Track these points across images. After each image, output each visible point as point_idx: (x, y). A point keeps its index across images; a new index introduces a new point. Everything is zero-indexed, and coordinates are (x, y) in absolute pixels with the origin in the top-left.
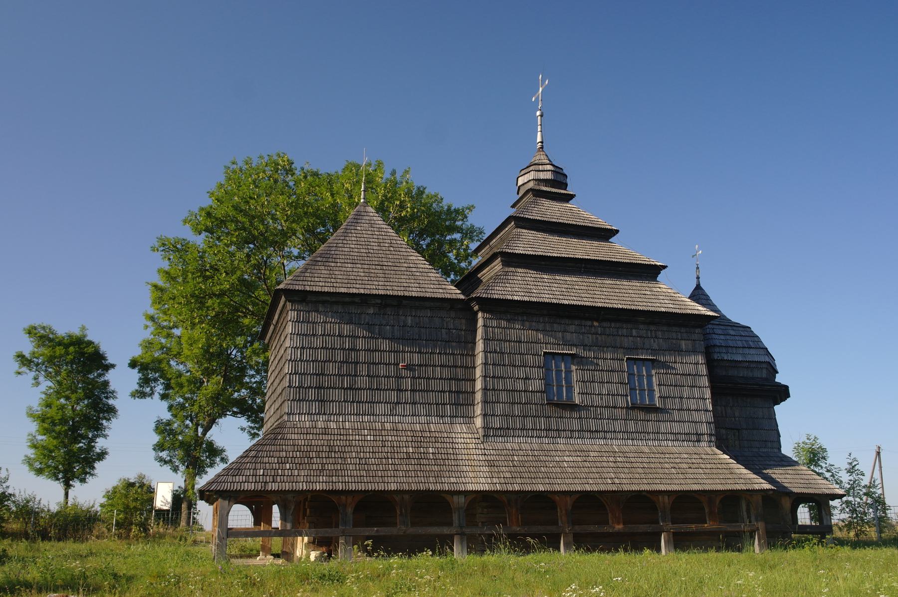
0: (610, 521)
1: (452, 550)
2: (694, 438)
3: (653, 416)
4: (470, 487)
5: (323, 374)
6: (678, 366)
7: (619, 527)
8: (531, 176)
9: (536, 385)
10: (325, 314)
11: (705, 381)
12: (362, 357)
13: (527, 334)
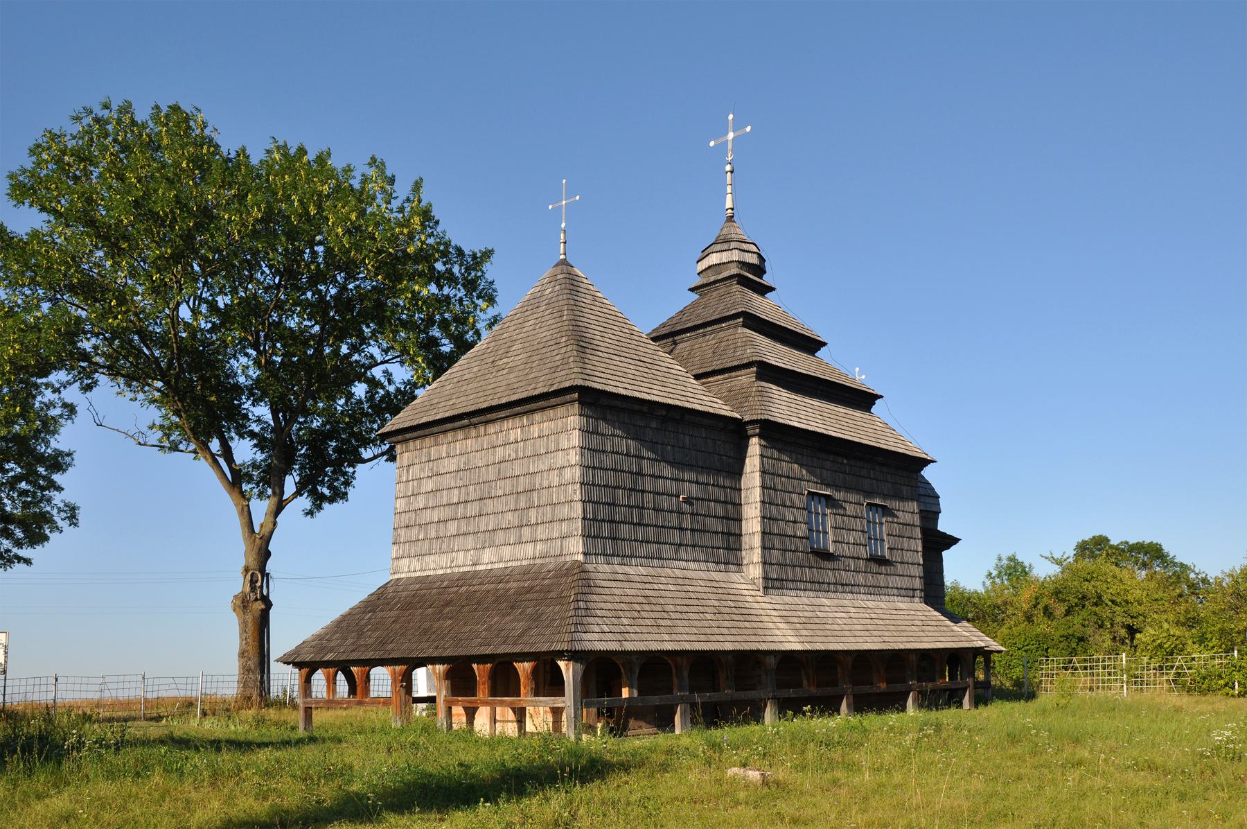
0: (805, 682)
2: (911, 593)
3: (883, 569)
4: (588, 646)
5: (614, 504)
6: (900, 514)
8: (735, 256)
9: (801, 530)
11: (918, 533)
12: (648, 483)
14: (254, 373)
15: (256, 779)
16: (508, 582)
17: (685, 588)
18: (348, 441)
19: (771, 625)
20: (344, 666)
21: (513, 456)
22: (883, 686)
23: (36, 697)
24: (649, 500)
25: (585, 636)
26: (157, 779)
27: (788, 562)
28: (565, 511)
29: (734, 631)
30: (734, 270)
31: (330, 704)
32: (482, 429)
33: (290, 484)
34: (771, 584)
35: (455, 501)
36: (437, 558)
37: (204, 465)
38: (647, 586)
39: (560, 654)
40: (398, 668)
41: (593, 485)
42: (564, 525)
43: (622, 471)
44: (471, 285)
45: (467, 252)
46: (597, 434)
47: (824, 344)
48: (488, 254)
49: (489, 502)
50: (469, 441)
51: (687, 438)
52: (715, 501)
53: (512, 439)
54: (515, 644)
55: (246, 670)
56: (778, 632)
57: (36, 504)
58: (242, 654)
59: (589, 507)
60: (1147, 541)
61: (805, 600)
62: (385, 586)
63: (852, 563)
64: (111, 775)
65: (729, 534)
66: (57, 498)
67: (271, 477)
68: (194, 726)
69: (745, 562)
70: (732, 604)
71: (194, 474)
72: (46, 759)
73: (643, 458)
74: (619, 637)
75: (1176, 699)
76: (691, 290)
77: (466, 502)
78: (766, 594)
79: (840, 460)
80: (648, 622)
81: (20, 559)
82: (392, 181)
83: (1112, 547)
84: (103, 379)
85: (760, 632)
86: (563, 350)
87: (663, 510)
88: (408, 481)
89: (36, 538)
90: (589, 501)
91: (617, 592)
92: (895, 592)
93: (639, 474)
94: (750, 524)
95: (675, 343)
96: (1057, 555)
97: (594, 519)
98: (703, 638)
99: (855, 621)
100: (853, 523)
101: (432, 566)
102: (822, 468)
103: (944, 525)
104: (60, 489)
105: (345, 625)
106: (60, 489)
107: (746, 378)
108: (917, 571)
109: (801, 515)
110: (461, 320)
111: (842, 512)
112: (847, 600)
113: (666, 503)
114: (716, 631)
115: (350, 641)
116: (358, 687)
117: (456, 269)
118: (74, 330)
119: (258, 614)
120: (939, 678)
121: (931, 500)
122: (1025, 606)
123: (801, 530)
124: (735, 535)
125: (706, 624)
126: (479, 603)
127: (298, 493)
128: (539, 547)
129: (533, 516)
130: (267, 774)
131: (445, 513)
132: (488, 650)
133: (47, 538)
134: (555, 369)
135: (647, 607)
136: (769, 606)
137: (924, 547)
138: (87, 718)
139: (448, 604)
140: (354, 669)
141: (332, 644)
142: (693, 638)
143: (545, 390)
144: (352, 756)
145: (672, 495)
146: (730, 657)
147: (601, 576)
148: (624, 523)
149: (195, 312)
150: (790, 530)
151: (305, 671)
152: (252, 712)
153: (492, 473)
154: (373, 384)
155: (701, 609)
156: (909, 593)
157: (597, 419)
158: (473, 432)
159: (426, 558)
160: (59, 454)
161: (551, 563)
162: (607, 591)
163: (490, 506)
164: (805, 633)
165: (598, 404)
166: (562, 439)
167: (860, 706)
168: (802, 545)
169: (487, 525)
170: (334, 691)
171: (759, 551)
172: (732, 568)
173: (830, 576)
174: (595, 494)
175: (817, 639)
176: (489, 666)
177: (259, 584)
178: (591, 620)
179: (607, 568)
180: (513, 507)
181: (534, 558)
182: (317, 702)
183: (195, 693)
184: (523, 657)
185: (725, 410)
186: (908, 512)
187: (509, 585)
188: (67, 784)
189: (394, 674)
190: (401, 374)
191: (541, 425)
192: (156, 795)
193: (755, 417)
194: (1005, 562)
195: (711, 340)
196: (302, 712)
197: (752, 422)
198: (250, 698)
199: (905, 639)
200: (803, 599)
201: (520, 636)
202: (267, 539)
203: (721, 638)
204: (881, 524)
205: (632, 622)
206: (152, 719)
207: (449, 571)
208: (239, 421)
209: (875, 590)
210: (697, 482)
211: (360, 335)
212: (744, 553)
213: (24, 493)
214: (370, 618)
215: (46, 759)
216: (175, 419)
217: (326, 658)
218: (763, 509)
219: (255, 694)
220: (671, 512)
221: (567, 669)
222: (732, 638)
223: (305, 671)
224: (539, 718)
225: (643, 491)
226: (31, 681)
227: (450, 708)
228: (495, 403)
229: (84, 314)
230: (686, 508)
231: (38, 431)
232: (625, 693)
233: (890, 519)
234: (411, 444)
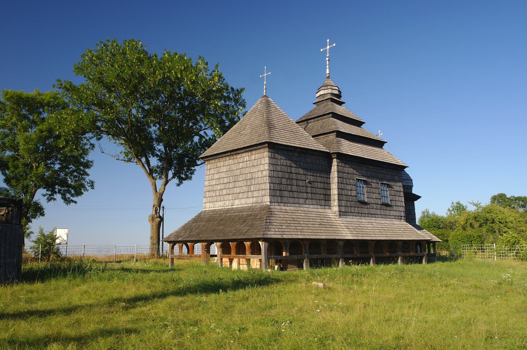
0: (355, 252)
1: (338, 265)
2: (400, 218)
3: (388, 208)
4: (269, 236)
6: (394, 187)
7: (388, 254)
8: (330, 91)
10: (280, 154)
11: (402, 194)
12: (294, 176)
13: (351, 170)
14: (158, 132)
15: (148, 282)
17: (308, 215)
18: (192, 158)
19: (341, 229)
20: (185, 243)
22: (388, 254)
23: (77, 253)
24: (294, 182)
25: (269, 233)
26: (115, 281)
28: (263, 186)
29: (326, 231)
30: (329, 96)
31: (180, 257)
32: (235, 156)
33: (170, 174)
34: (341, 214)
36: (219, 203)
37: (139, 166)
39: (259, 239)
40: (204, 244)
44: (236, 101)
45: (235, 89)
47: (364, 123)
48: (242, 90)
51: (309, 160)
52: (320, 182)
53: (245, 160)
54: (244, 235)
55: (153, 244)
56: (344, 232)
57: (80, 181)
58: (151, 238)
59: (272, 185)
60: (523, 196)
61: (356, 220)
62: (201, 213)
63: (375, 206)
64: (100, 280)
65: (326, 195)
66: (87, 178)
67: (163, 171)
68: (132, 265)
70: (326, 221)
71: (136, 171)
72: (80, 273)
75: (517, 263)
76: (314, 104)
78: (340, 218)
79: (369, 167)
80: (293, 228)
81: (73, 201)
82: (207, 64)
83: (507, 198)
84: (104, 136)
85: (337, 232)
89: (79, 193)
91: (282, 216)
92: (393, 217)
93: (291, 173)
95: (308, 123)
96: (475, 202)
97: (274, 189)
98: (314, 234)
99: (376, 228)
101: (217, 206)
102: (362, 170)
103: (415, 191)
104: (88, 175)
105: (186, 227)
106: (88, 175)
107: (332, 137)
108: (403, 209)
109: (354, 188)
110: (234, 112)
111: (370, 186)
112: (373, 220)
114: (319, 231)
115: (187, 234)
116: (190, 250)
117: (231, 95)
118: (95, 120)
119: (158, 222)
120: (413, 252)
121: (409, 181)
122: (462, 223)
123: (354, 193)
124: (328, 195)
125: (315, 228)
126: (233, 220)
127: (173, 177)
128: (255, 199)
129: (252, 188)
130: (152, 280)
131: (222, 186)
132: (235, 237)
133: (82, 193)
134: (260, 136)
135: (293, 222)
136: (341, 222)
137: (405, 200)
138: (94, 261)
139: (222, 220)
140: (189, 244)
141: (181, 234)
142: (310, 234)
143: (256, 143)
144: (183, 275)
146: (325, 241)
147: (276, 210)
149: (138, 112)
150: (349, 193)
151: (172, 244)
152: (155, 260)
153: (238, 172)
154: (201, 137)
155: (314, 223)
156: (399, 218)
158: (232, 157)
160: (88, 161)
161: (258, 205)
162: (278, 216)
163: (238, 184)
164: (355, 232)
165: (274, 148)
166: (262, 160)
167: (378, 262)
168: (354, 199)
170: (182, 252)
171: (337, 201)
172: (327, 207)
173: (366, 211)
174: (274, 180)
176: (235, 243)
178: (271, 227)
179: (278, 207)
182: (176, 256)
183: (135, 254)
184: (247, 240)
185: (323, 149)
186: (398, 187)
188: (86, 282)
189: (202, 245)
190: (210, 133)
191: (255, 155)
192: (115, 286)
193: (334, 152)
194: (455, 204)
195: (320, 122)
196: (170, 260)
198: (154, 255)
200: (355, 219)
201: (246, 232)
202: (162, 195)
203: (321, 234)
204: (387, 191)
205: (287, 227)
206: (118, 262)
208: (152, 150)
209: (384, 216)
210: (313, 176)
211: (196, 119)
213: (75, 176)
215: (80, 273)
216: (130, 150)
218: (338, 185)
219: (156, 254)
222: (325, 234)
223: (172, 244)
224: (255, 263)
225: (292, 179)
226: (76, 247)
227: (222, 259)
228: (239, 147)
229: (98, 114)
230: (309, 185)
231: (81, 154)
232: (284, 254)
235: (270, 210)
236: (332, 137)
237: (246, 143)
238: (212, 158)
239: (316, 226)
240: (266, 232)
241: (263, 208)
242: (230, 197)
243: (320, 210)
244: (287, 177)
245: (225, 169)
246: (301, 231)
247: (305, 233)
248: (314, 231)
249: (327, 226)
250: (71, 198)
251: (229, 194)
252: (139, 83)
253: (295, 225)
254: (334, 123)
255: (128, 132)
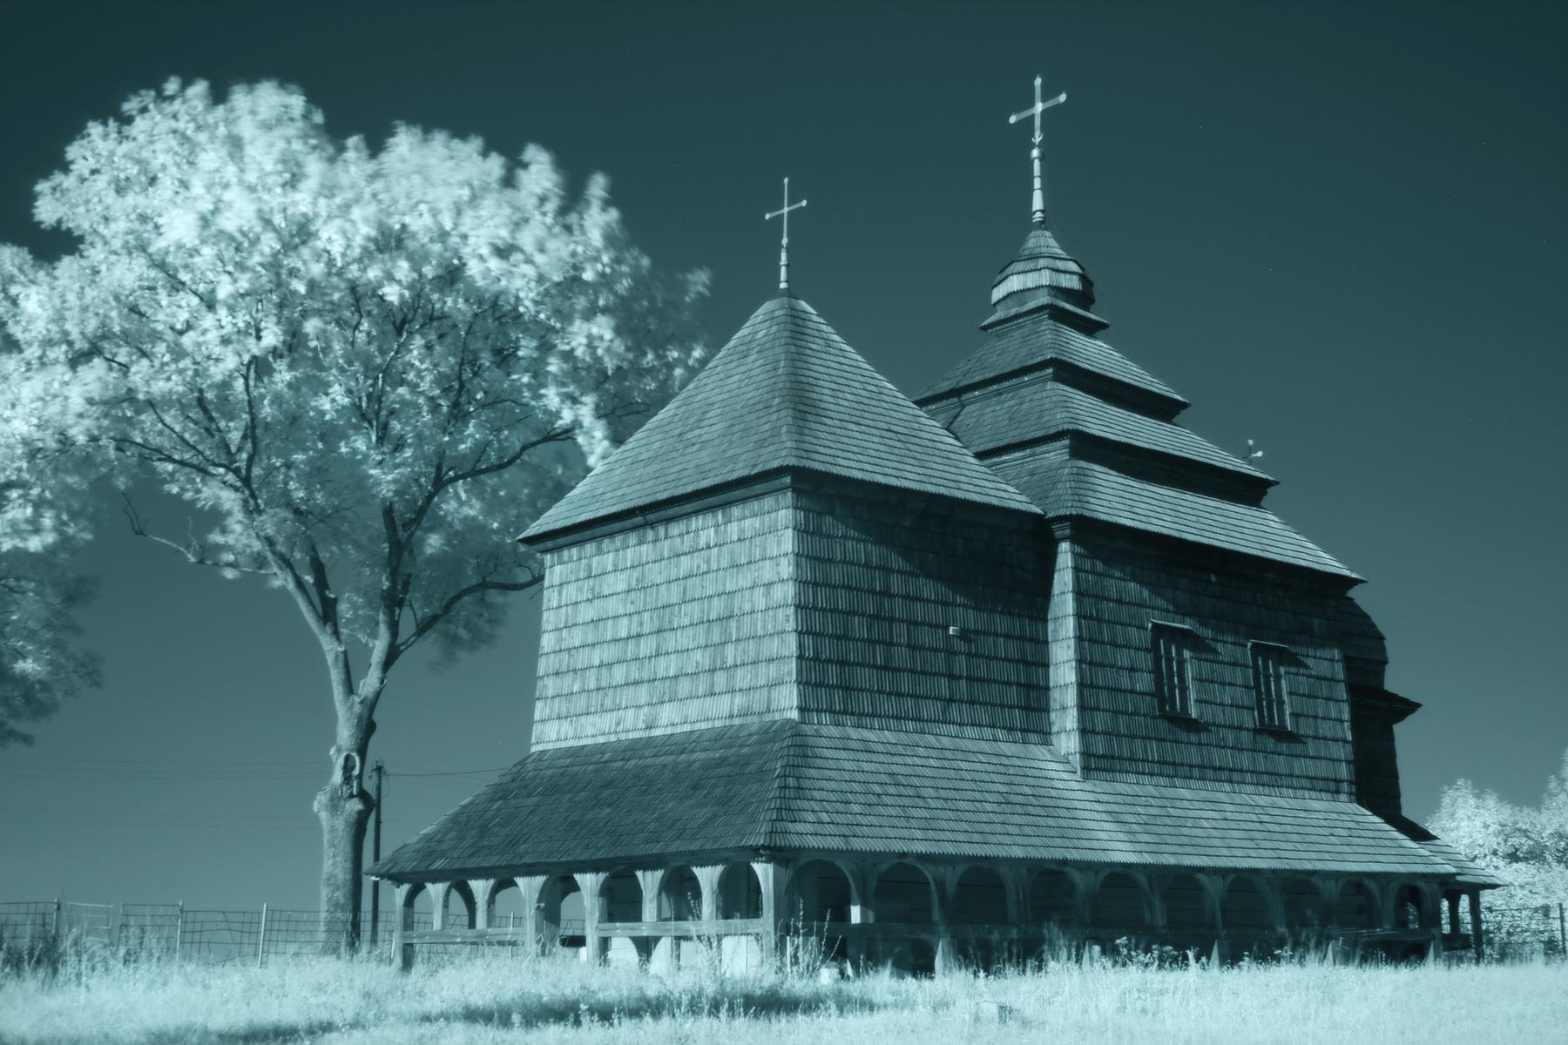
2: (1333, 786)
3: (1284, 747)
4: (796, 841)
6: (1310, 662)
8: (1045, 278)
9: (1144, 682)
11: (1341, 691)
12: (899, 608)
16: (693, 751)
21: (704, 568)
24: (900, 633)
25: (791, 827)
27: (1123, 730)
28: (773, 647)
29: (1028, 830)
30: (1044, 299)
34: (1094, 764)
35: (624, 634)
36: (596, 719)
38: (895, 759)
41: (815, 608)
42: (773, 668)
43: (858, 589)
46: (821, 534)
49: (668, 635)
50: (644, 548)
53: (702, 543)
54: (693, 838)
63: (1230, 737)
69: (1055, 729)
73: (891, 571)
74: (845, 830)
77: (639, 636)
78: (1086, 778)
80: (892, 811)
81: (12, 733)
86: (774, 417)
87: (922, 648)
88: (560, 607)
90: (808, 633)
93: (886, 593)
94: (1061, 672)
98: (976, 837)
99: (1233, 825)
100: (1228, 673)
101: (590, 731)
103: (1395, 682)
107: (1056, 454)
108: (1342, 752)
111: (1211, 657)
113: (927, 638)
114: (999, 828)
124: (1038, 687)
125: (984, 817)
128: (739, 701)
129: (730, 653)
131: (610, 653)
132: (656, 849)
134: (761, 444)
135: (892, 790)
139: (607, 785)
141: (444, 846)
142: (961, 837)
145: (936, 626)
147: (824, 742)
148: (862, 665)
150: (1125, 682)
155: (978, 796)
156: (1331, 787)
157: (820, 514)
158: (650, 534)
159: (583, 719)
162: (832, 764)
163: (671, 641)
165: (821, 494)
169: (667, 669)
172: (1033, 737)
174: (817, 623)
175: (1165, 848)
177: (356, 772)
178: (805, 804)
180: (702, 643)
181: (731, 717)
185: (1014, 498)
186: (1327, 663)
187: (694, 756)
191: (742, 522)
193: (1062, 512)
197: (1060, 519)
199: (1314, 856)
200: (1149, 788)
201: (701, 828)
203: (1007, 839)
205: (867, 810)
207: (613, 738)
209: (1271, 780)
212: (1053, 716)
214: (499, 809)
215: (39, 962)
217: (434, 867)
220: (936, 650)
221: (764, 871)
230: (961, 646)
232: (856, 914)
233: (1293, 670)
234: (566, 553)
235: (798, 740)
236: (1056, 454)
237: (703, 474)
238: (570, 538)
239: (988, 807)
240: (780, 826)
241: (771, 733)
242: (643, 694)
243: (1006, 748)
244: (871, 610)
245: (620, 582)
246: (923, 824)
247: (942, 835)
248: (978, 827)
249: (1031, 810)
250: (12, 723)
251: (636, 683)
252: (289, 247)
253: (899, 801)
254: (1065, 404)
255: (240, 449)
